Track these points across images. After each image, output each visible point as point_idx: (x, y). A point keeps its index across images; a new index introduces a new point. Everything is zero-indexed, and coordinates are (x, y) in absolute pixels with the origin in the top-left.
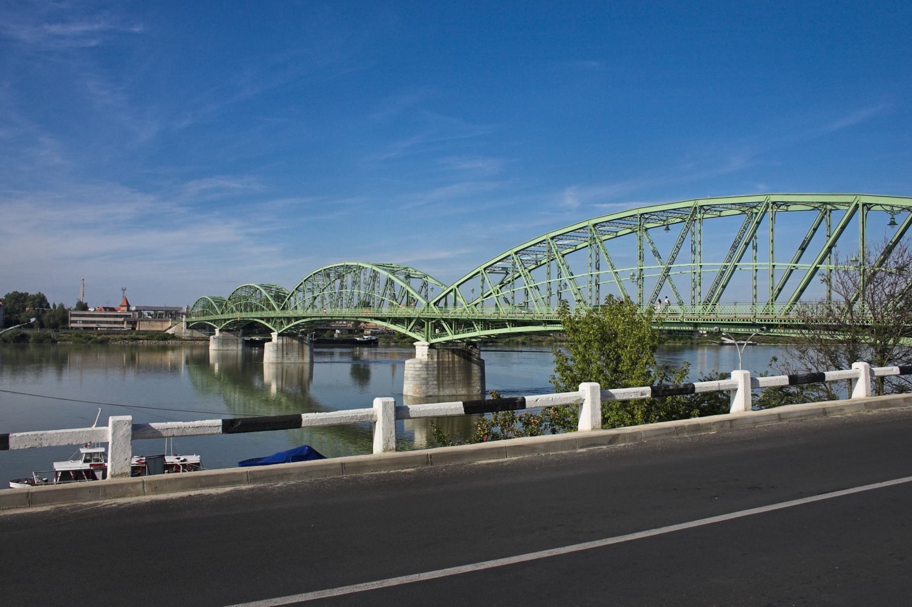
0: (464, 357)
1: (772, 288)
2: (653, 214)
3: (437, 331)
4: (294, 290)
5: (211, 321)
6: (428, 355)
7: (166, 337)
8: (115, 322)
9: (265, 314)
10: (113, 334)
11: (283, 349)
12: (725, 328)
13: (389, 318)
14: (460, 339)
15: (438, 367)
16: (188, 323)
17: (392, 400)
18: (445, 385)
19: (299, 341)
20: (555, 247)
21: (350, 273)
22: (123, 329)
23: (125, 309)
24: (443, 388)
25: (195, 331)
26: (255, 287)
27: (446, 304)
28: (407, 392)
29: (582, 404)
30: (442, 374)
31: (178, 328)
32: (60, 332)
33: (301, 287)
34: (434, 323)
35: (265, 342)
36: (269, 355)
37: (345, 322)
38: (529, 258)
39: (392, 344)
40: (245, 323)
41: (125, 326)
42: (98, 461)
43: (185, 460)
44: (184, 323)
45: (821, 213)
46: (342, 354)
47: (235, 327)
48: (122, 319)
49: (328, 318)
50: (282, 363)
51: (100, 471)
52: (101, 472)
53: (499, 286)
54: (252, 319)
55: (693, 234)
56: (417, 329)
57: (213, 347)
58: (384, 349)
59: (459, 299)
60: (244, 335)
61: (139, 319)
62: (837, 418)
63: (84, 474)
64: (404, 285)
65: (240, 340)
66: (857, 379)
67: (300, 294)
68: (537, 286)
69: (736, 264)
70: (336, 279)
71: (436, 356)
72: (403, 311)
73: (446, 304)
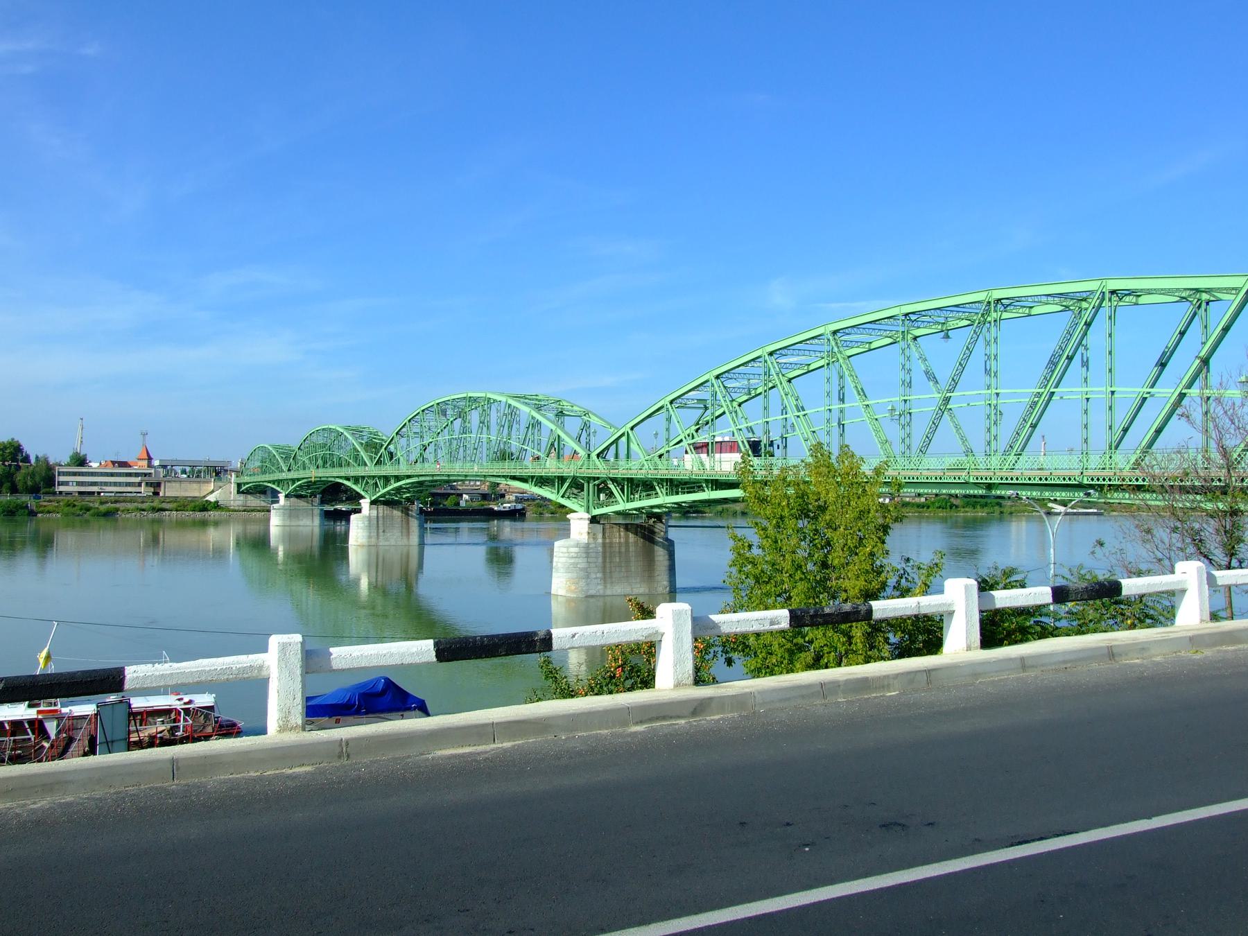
0: (644, 537)
1: (1110, 427)
2: (923, 313)
3: (602, 496)
4: (394, 434)
5: (273, 482)
6: (589, 533)
7: (205, 507)
8: (128, 484)
9: (352, 472)
10: (124, 501)
11: (378, 524)
12: (1065, 491)
13: (533, 477)
14: (635, 509)
15: (604, 552)
16: (239, 485)
17: (298, 638)
18: (614, 580)
19: (402, 513)
20: (774, 368)
21: (476, 408)
22: (139, 495)
23: (145, 463)
24: (612, 583)
25: (249, 497)
26: (338, 431)
27: (617, 456)
28: (557, 590)
29: (661, 641)
30: (610, 562)
31: (222, 493)
32: (42, 500)
33: (404, 430)
34: (598, 485)
35: (351, 514)
36: (358, 533)
37: (478, 483)
38: (736, 384)
39: (547, 515)
40: (325, 484)
41: (142, 489)
42: (51, 706)
43: (190, 702)
44: (233, 485)
45: (1192, 307)
46: (471, 530)
47: (310, 491)
48: (138, 480)
49: (442, 478)
50: (377, 546)
51: (53, 721)
52: (55, 723)
53: (694, 428)
54: (333, 479)
55: (988, 343)
56: (573, 494)
57: (276, 522)
58: (535, 523)
59: (634, 446)
60: (323, 502)
61: (165, 479)
62: (1132, 666)
63: (27, 726)
64: (553, 427)
65: (317, 511)
66: (1183, 591)
67: (403, 441)
68: (751, 427)
69: (1052, 390)
70: (456, 419)
71: (600, 536)
72: (551, 467)
73: (617, 456)
